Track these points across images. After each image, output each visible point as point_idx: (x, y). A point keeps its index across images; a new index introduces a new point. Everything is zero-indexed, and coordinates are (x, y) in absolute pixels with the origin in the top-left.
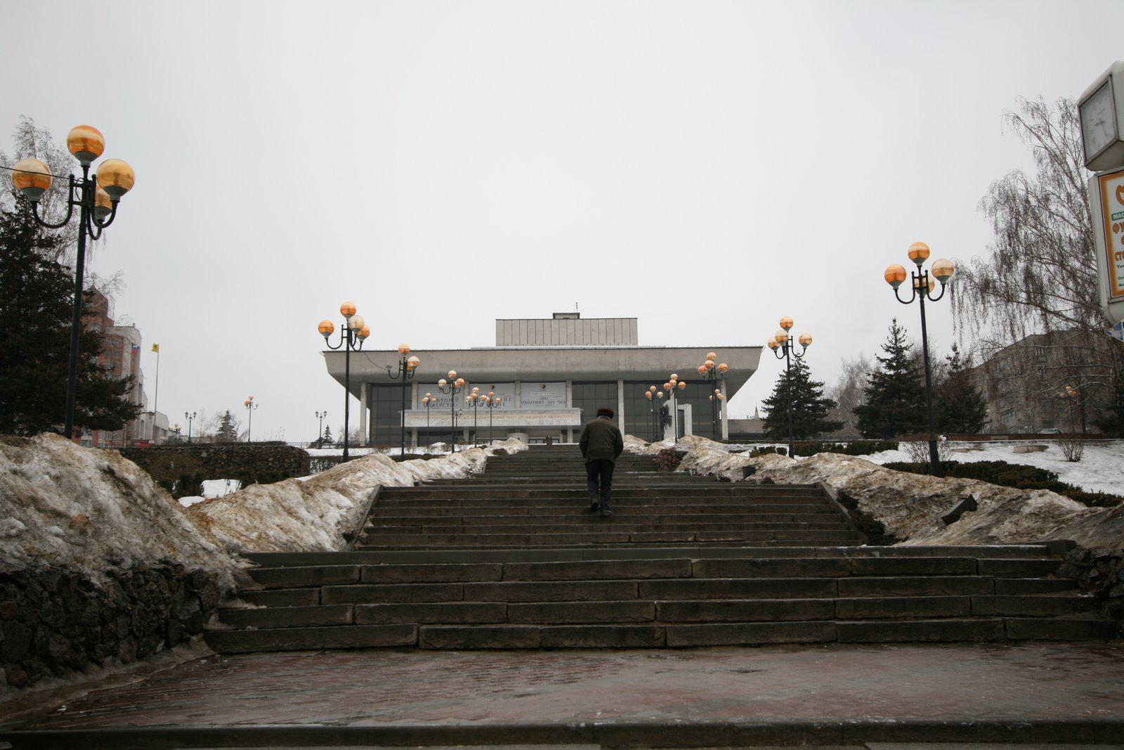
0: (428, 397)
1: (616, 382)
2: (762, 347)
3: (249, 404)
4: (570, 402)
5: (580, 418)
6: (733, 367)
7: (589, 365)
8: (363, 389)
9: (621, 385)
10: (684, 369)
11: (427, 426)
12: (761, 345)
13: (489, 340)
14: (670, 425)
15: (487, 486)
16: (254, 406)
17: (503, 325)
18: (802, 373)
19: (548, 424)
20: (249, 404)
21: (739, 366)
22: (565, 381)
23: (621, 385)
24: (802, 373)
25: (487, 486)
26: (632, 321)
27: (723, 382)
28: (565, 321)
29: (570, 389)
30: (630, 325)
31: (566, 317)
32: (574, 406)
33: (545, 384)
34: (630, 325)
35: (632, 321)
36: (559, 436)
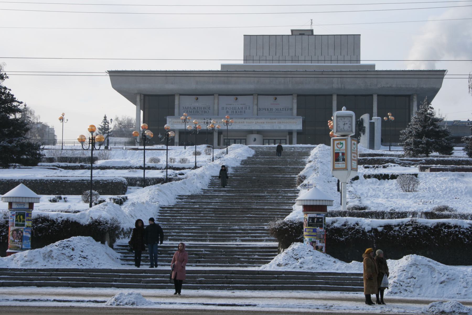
0: (185, 116)
1: (331, 95)
2: (445, 71)
3: (62, 119)
4: (295, 111)
5: (301, 124)
6: (421, 86)
7: (311, 85)
8: (138, 99)
9: (335, 98)
10: (384, 87)
11: (184, 128)
12: (445, 69)
13: (236, 57)
14: (364, 133)
15: (184, 217)
16: (65, 120)
17: (250, 41)
18: (428, 111)
19: (278, 128)
20: (62, 119)
21: (426, 84)
22: (292, 95)
23: (335, 98)
24: (428, 111)
25: (184, 217)
26: (356, 39)
27: (415, 97)
28: (300, 36)
29: (295, 101)
30: (352, 43)
31: (302, 33)
32: (298, 114)
33: (277, 97)
34: (352, 43)
35: (356, 39)
36: (286, 137)
